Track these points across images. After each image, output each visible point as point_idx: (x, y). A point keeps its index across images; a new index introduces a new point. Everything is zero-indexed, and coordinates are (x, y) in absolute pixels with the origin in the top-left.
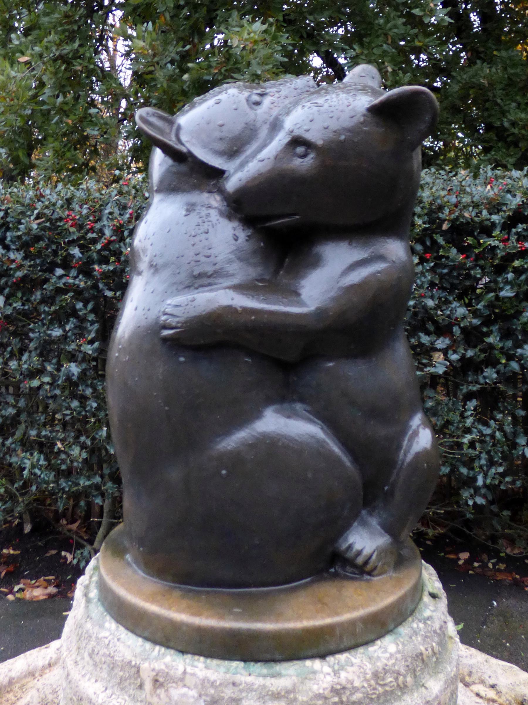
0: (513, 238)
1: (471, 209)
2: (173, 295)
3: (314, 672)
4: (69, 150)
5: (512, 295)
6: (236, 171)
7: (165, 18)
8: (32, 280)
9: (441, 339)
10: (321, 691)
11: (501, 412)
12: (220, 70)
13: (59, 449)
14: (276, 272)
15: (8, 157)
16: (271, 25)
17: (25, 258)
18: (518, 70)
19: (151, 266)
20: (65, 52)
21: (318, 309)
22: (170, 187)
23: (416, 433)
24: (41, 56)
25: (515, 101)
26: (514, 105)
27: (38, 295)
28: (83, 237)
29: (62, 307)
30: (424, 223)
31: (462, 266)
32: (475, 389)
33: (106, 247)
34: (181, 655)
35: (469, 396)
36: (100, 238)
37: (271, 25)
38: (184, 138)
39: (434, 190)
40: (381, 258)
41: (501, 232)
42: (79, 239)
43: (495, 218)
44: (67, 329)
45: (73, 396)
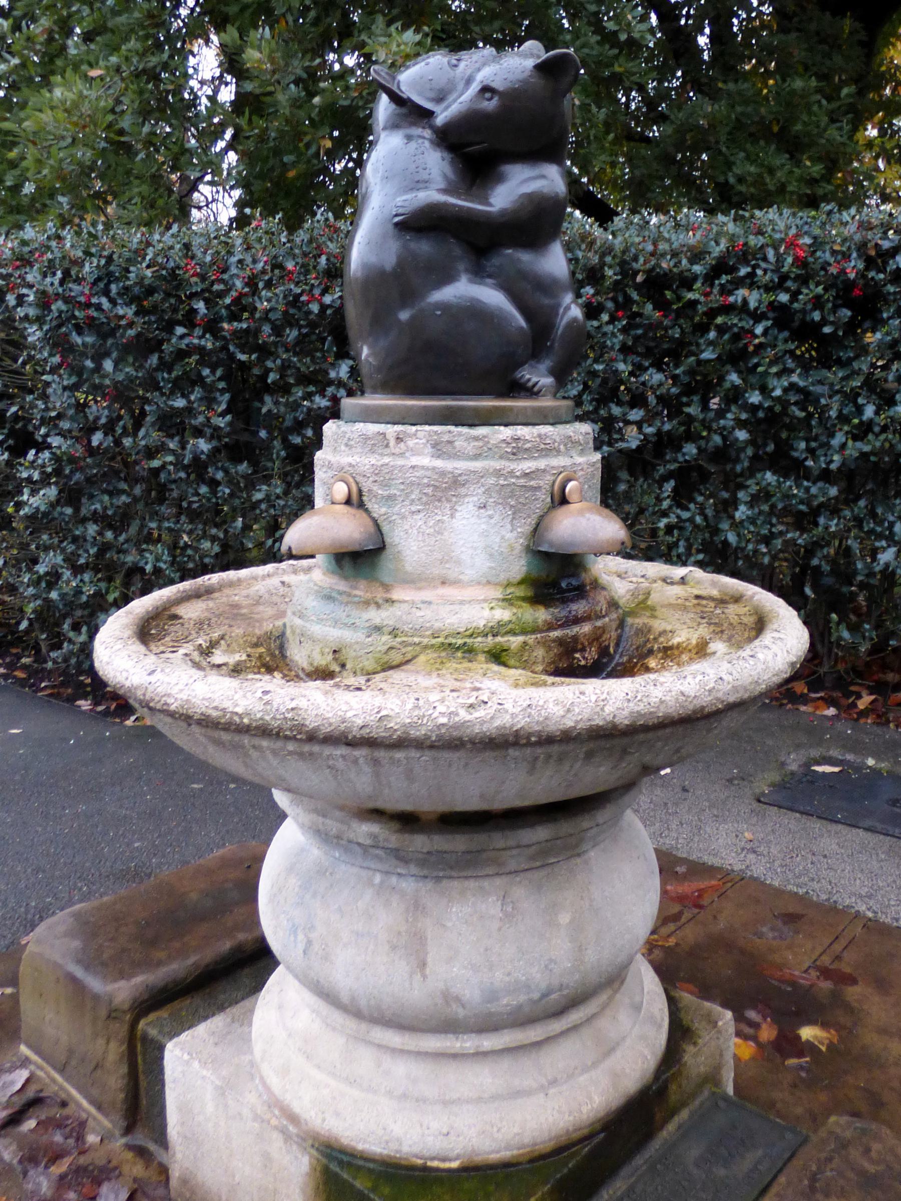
0: (716, 290)
1: (669, 257)
2: (401, 195)
4: (161, 197)
5: (713, 356)
6: (442, 112)
7: (287, 22)
8: (148, 340)
9: (635, 410)
11: (702, 494)
12: (360, 94)
13: (185, 543)
15: (71, 208)
16: (426, 35)
17: (136, 314)
18: (749, 109)
20: (151, 64)
22: (393, 126)
24: (118, 70)
25: (745, 151)
26: (742, 155)
27: (154, 360)
28: (208, 290)
29: (185, 373)
30: (615, 274)
31: (659, 325)
32: (672, 468)
33: (237, 301)
35: (665, 478)
36: (230, 290)
37: (427, 35)
38: (403, 89)
39: (627, 235)
40: (543, 177)
41: (703, 284)
42: (203, 290)
43: (697, 268)
44: (193, 398)
45: (201, 478)
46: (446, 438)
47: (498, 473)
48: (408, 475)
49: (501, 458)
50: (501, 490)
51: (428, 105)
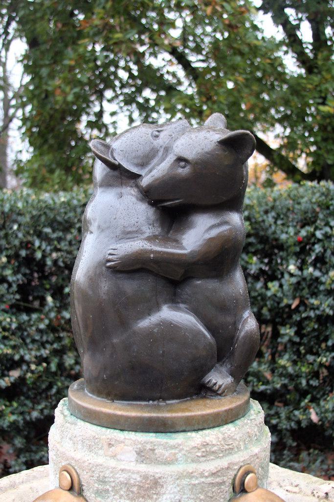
3: (193, 438)
6: (146, 175)
10: (196, 445)
14: (168, 232)
19: (99, 227)
21: (191, 251)
22: (107, 184)
23: (246, 320)
34: (122, 432)
38: (115, 155)
40: (226, 223)
46: (148, 447)
47: (190, 475)
48: (118, 476)
49: (193, 461)
50: (192, 488)
51: (134, 170)
